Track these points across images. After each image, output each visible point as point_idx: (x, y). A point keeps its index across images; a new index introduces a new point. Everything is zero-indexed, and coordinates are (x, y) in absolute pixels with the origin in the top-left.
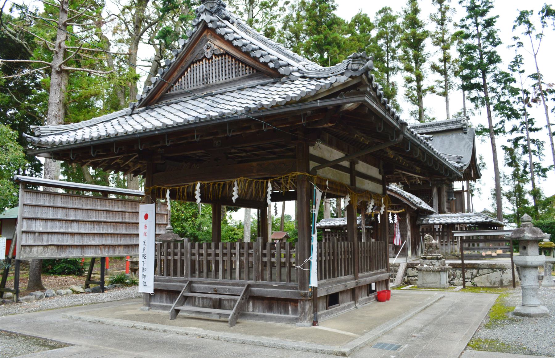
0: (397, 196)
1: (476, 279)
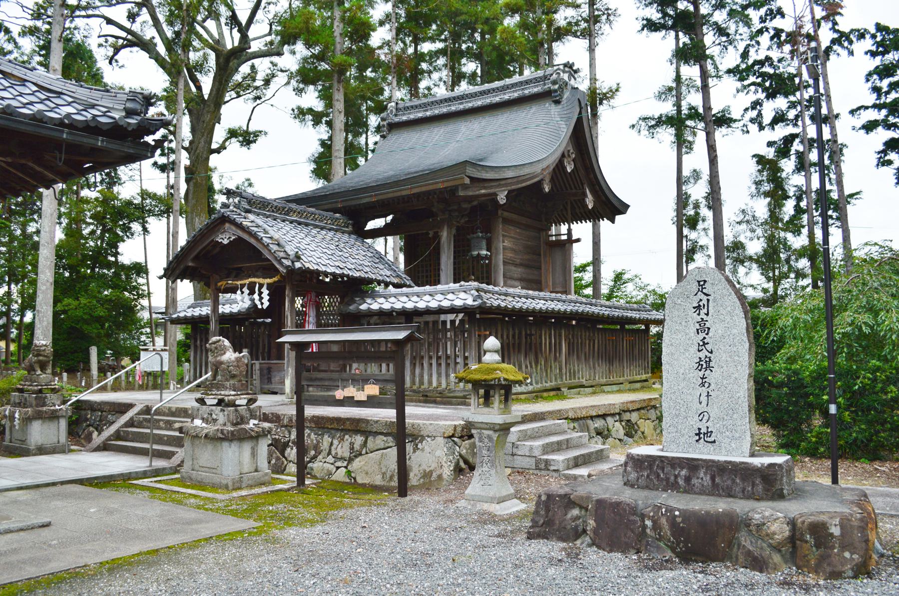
0: (252, 241)
1: (357, 464)
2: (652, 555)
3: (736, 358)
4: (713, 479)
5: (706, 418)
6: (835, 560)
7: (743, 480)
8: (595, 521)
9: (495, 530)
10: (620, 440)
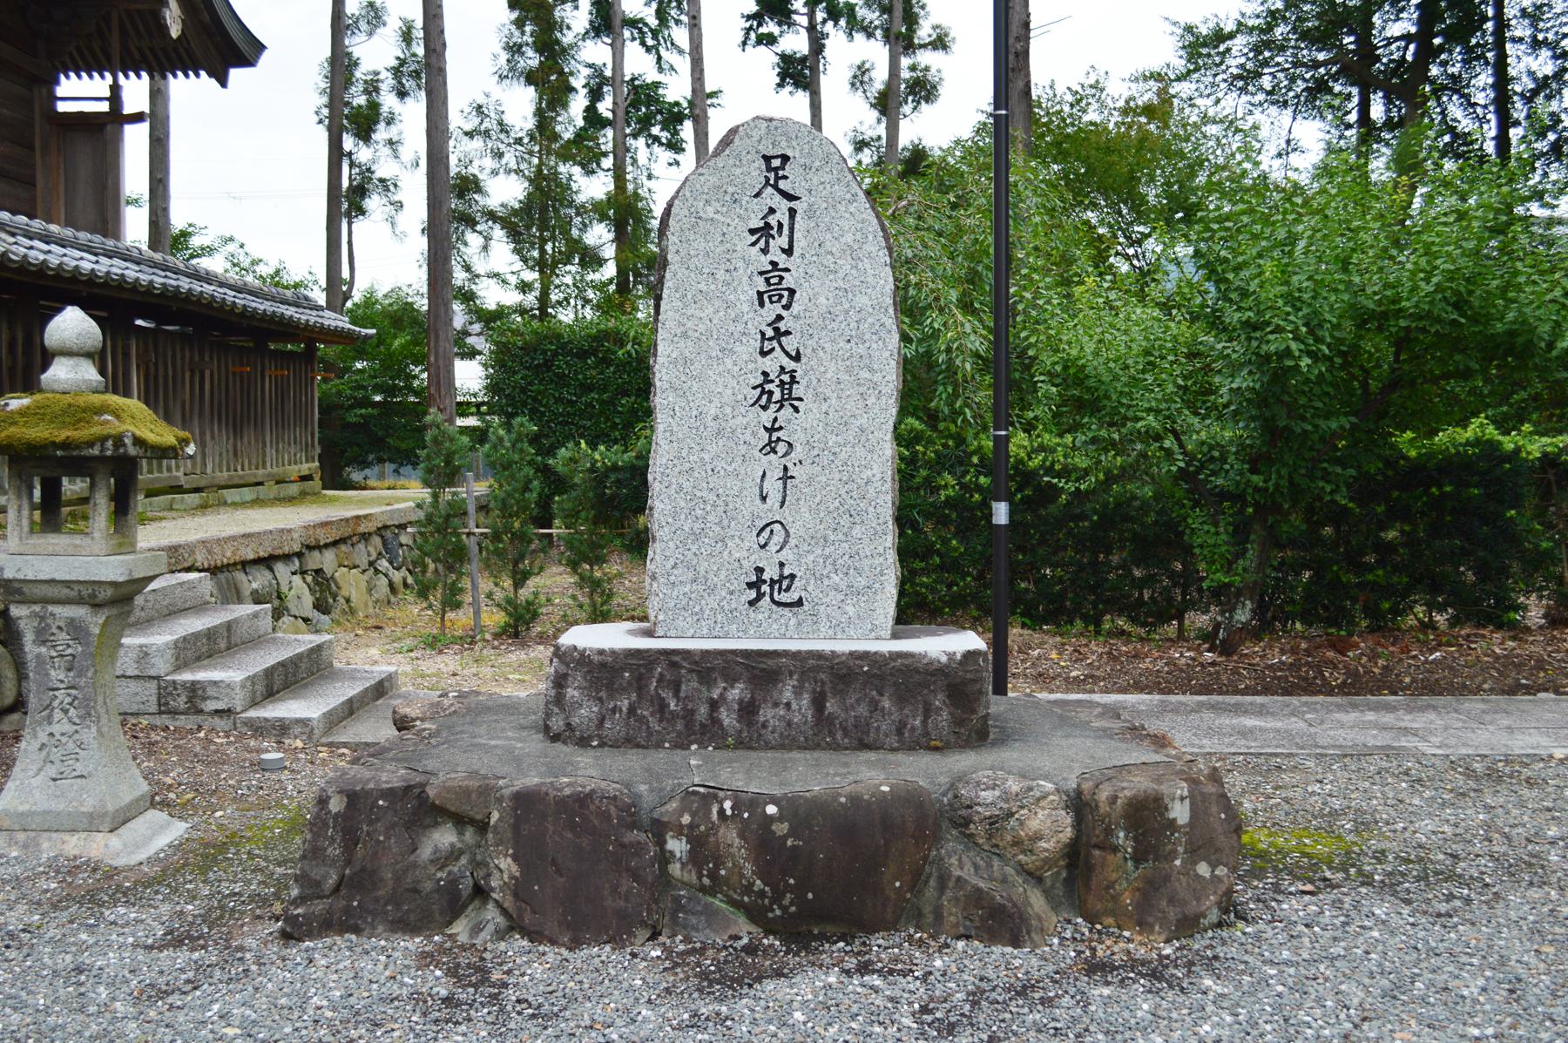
2: (698, 937)
3: (865, 374)
4: (818, 703)
5: (778, 538)
6: (1180, 885)
7: (901, 700)
8: (515, 858)
9: (155, 917)
10: (306, 620)
